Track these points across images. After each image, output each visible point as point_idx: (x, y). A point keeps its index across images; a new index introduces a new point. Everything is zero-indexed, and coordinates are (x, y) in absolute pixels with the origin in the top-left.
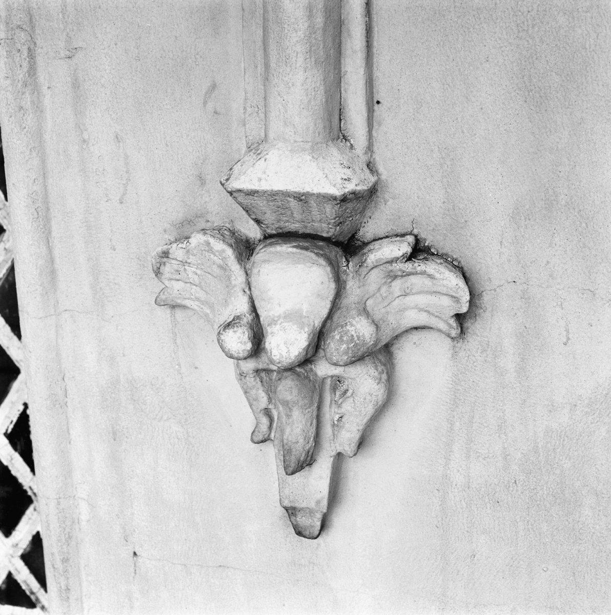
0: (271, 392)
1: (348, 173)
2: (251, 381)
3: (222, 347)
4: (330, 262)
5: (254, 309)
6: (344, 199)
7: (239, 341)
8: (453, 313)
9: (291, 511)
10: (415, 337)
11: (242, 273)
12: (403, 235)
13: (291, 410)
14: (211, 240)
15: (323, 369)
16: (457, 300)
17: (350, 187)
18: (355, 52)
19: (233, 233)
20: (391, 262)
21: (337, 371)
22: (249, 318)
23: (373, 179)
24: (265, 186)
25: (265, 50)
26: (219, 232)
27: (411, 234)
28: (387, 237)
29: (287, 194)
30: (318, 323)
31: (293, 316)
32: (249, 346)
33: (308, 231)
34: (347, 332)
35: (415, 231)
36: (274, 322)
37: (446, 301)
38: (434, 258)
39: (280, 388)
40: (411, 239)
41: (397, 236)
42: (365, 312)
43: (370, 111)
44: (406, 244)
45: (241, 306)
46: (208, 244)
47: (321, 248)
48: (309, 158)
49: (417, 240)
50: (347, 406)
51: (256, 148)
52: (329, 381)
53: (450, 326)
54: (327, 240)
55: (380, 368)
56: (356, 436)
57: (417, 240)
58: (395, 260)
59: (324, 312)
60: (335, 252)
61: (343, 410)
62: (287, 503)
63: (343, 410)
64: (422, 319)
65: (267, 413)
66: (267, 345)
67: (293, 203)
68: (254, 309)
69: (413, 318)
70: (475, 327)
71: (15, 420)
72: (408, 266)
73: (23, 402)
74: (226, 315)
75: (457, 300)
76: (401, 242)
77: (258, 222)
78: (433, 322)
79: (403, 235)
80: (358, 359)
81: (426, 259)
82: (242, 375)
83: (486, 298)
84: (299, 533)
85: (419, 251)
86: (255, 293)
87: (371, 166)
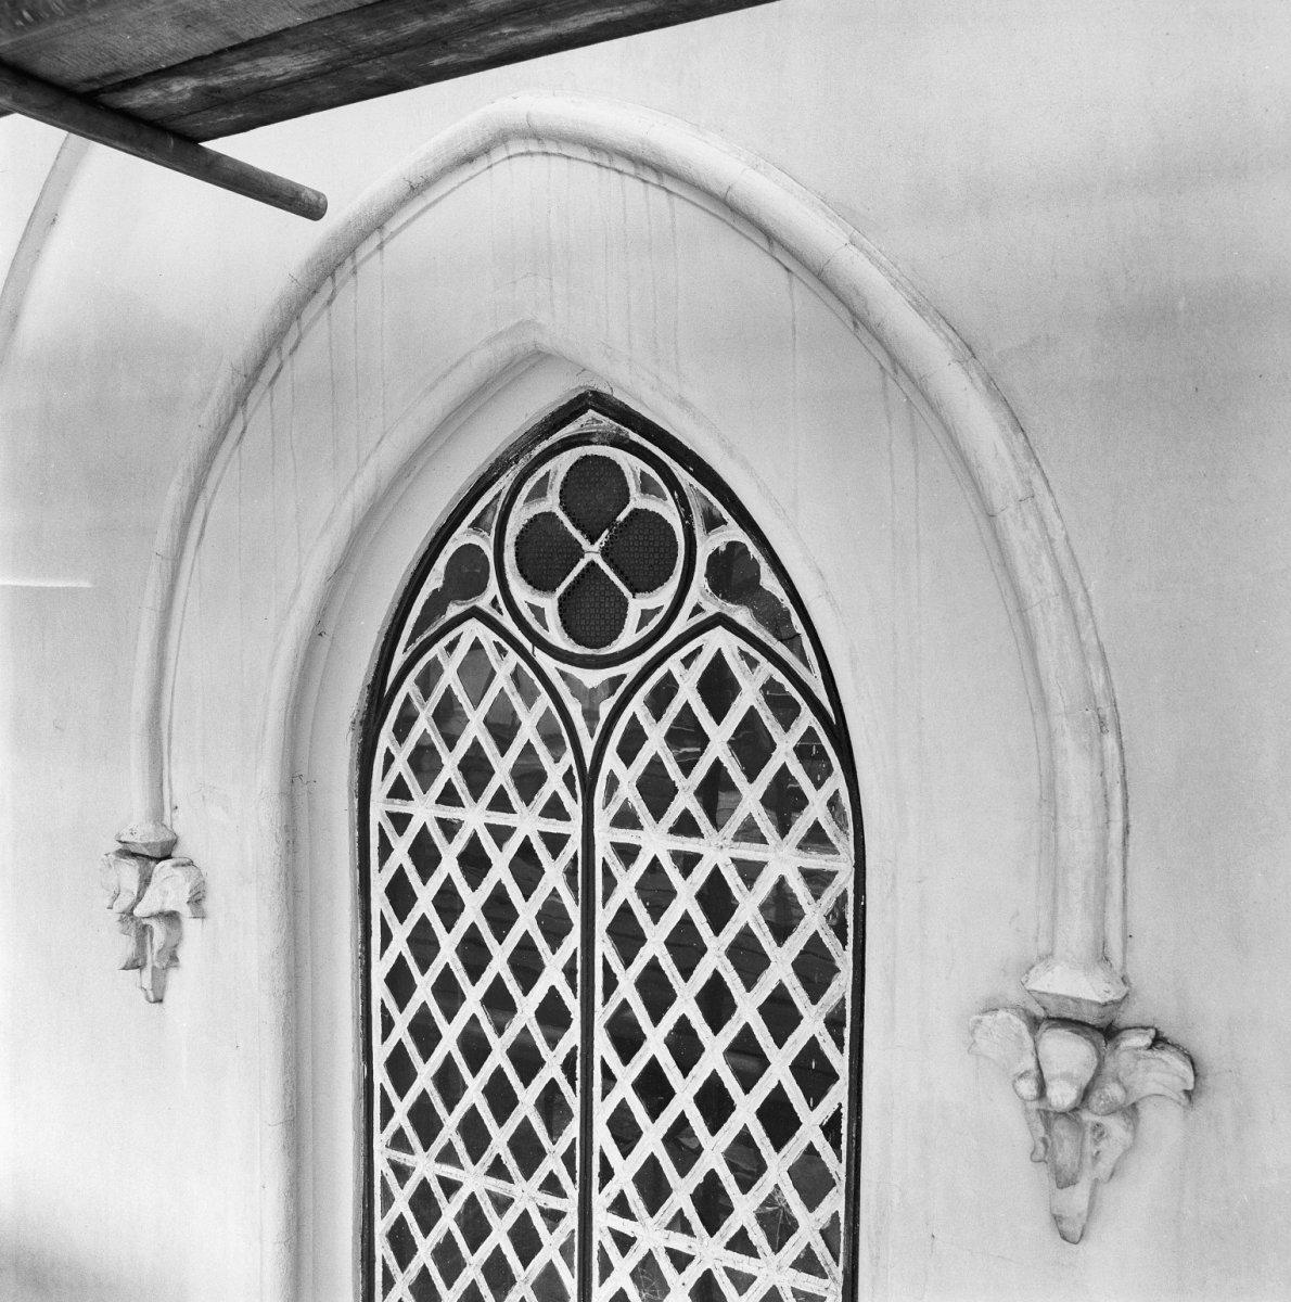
0: (1048, 1127)
1: (1109, 987)
2: (1034, 1116)
3: (1016, 1091)
4: (1094, 1043)
5: (1039, 1067)
6: (1106, 1005)
7: (1028, 1088)
8: (1182, 1088)
9: (1057, 1219)
10: (1155, 1100)
11: (1031, 1041)
12: (1146, 1028)
13: (1063, 1141)
14: (1012, 1017)
15: (1087, 1117)
16: (1184, 1080)
17: (1110, 997)
18: (1115, 905)
19: (1025, 1011)
20: (1137, 1049)
21: (1097, 1119)
22: (1035, 1073)
23: (1125, 989)
24: (1052, 990)
25: (880, 341)
26: (1015, 1008)
27: (1152, 1027)
28: (1135, 1028)
29: (1067, 997)
30: (1084, 1084)
31: (1067, 1077)
32: (1035, 1093)
33: (1079, 1019)
34: (1104, 1093)
35: (1156, 1026)
36: (1053, 1078)
37: (1177, 1080)
38: (1169, 1047)
39: (1056, 1125)
40: (1152, 1032)
41: (1143, 1027)
42: (1118, 1080)
43: (1125, 942)
44: (1148, 1037)
45: (1030, 1064)
46: (1009, 1019)
47: (1087, 1033)
48: (1082, 974)
49: (1157, 1032)
50: (1103, 1145)
51: (1047, 957)
52: (1090, 1125)
53: (1181, 1098)
54: (1093, 1027)
55: (1128, 1121)
56: (1109, 1170)
57: (1157, 1032)
58: (1140, 1048)
59: (1089, 1077)
60: (1098, 1037)
61: (1099, 1148)
62: (1055, 1212)
63: (1099, 1148)
64: (1160, 1090)
65: (1044, 1141)
66: (1048, 1094)
67: (1071, 1003)
68: (1039, 1067)
69: (1151, 1088)
70: (1201, 1100)
71: (830, 1115)
72: (1149, 1053)
73: (208, 921)
74: (1019, 1069)
75: (1184, 1080)
76: (1145, 1034)
77: (1044, 1009)
78: (1167, 1092)
79: (1146, 1028)
80: (1110, 1113)
81: (1163, 1048)
82: (1027, 1111)
83: (1209, 1081)
84: (1064, 1238)
85: (1159, 1041)
86: (1041, 1057)
87: (1124, 980)
